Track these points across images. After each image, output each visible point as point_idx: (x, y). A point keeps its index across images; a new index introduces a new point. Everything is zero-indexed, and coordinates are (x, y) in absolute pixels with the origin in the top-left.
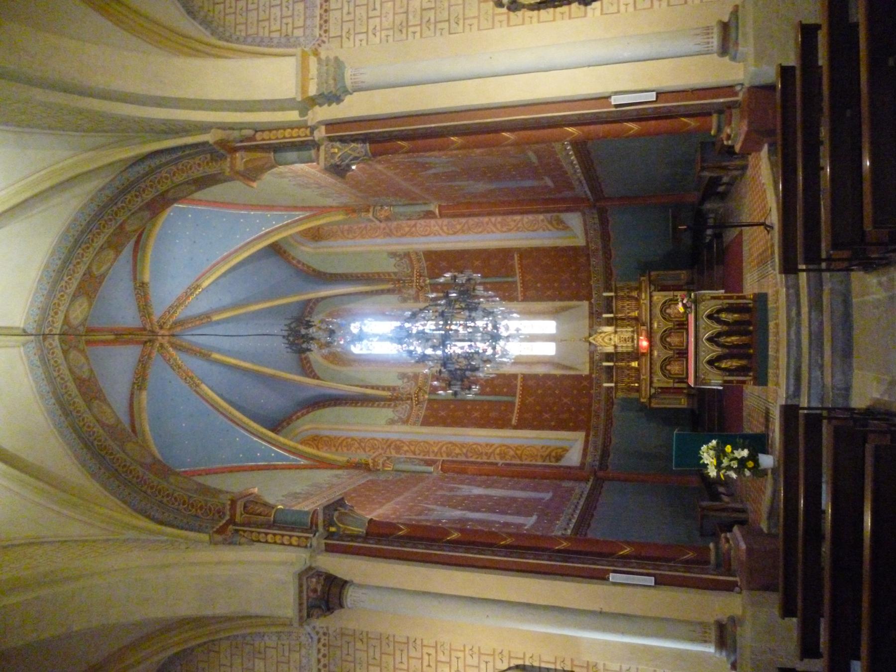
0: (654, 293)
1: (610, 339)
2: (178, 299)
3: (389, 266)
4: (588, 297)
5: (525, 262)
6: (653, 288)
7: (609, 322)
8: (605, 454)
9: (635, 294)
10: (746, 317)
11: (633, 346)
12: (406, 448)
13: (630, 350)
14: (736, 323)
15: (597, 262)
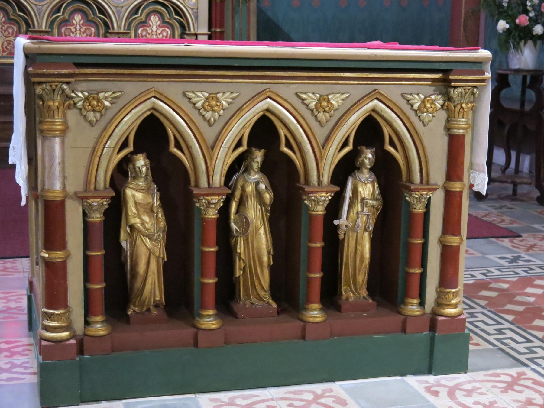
10: (356, 282)
14: (333, 242)
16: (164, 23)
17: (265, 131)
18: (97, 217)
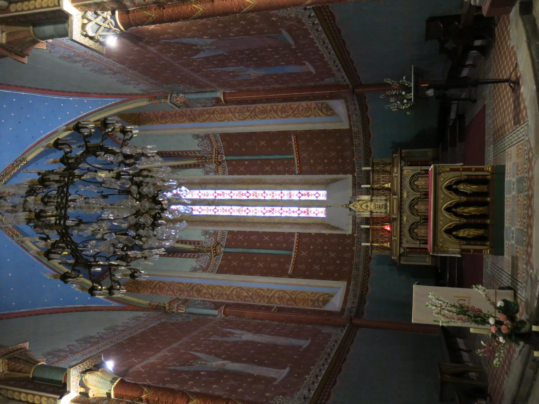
0: (404, 168)
1: (367, 206)
2: (6, 170)
3: (194, 146)
4: (352, 172)
5: (300, 142)
6: (403, 163)
7: (368, 192)
8: (362, 301)
9: (388, 168)
10: (484, 188)
11: (386, 212)
12: (205, 291)
13: (383, 215)
14: (474, 194)
15: (359, 141)
16: (417, 180)
17: (448, 210)
18: (465, 243)
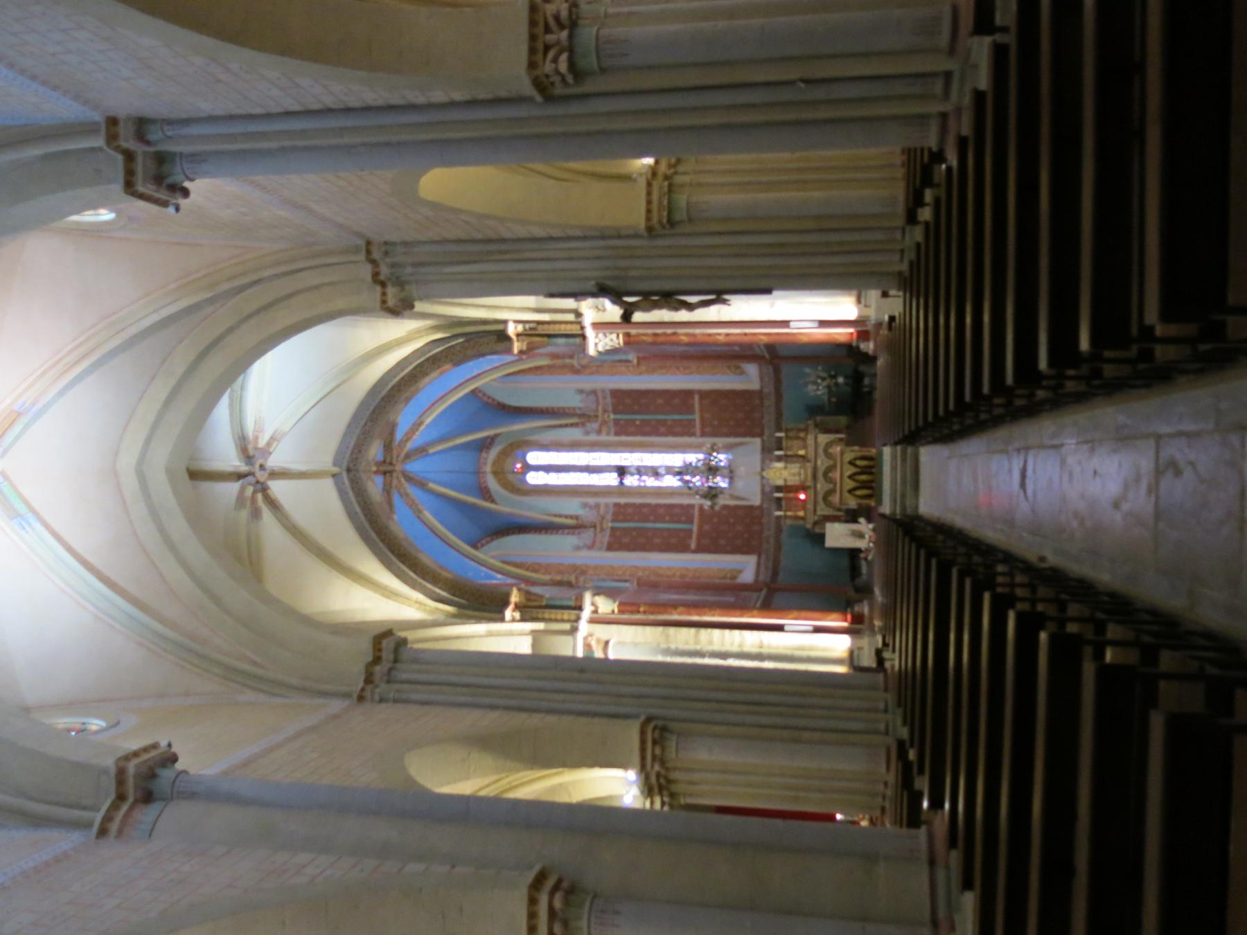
1: (781, 473)
3: (575, 402)
4: (761, 435)
7: (779, 459)
8: (775, 573)
10: (871, 463)
15: (770, 402)
